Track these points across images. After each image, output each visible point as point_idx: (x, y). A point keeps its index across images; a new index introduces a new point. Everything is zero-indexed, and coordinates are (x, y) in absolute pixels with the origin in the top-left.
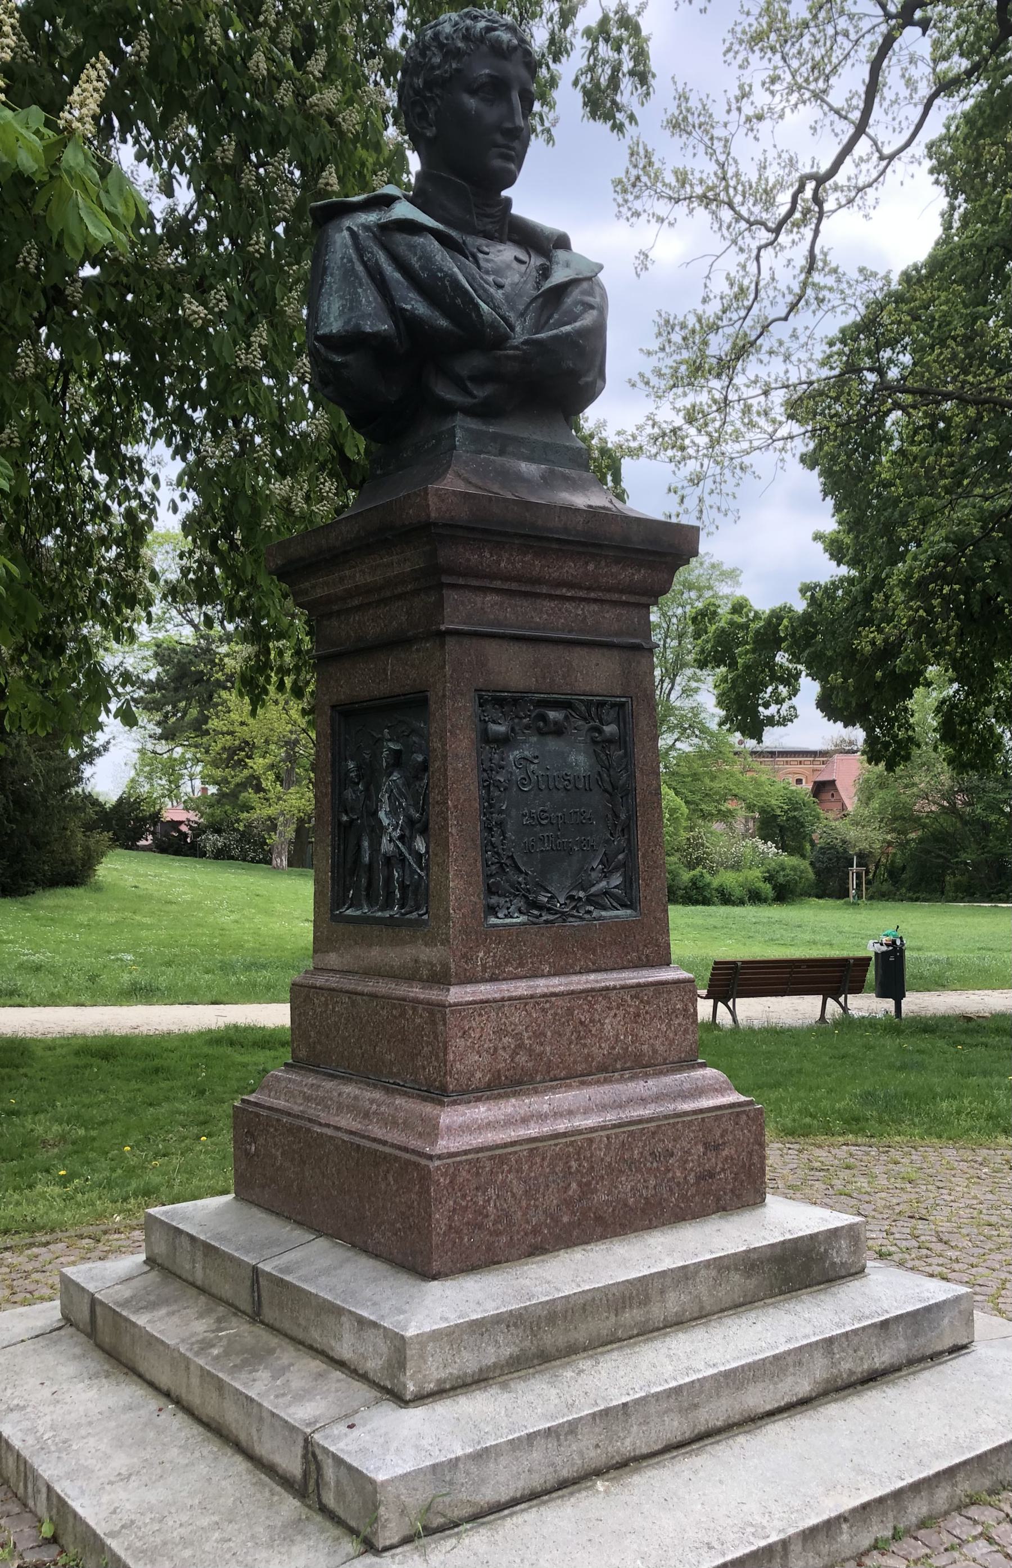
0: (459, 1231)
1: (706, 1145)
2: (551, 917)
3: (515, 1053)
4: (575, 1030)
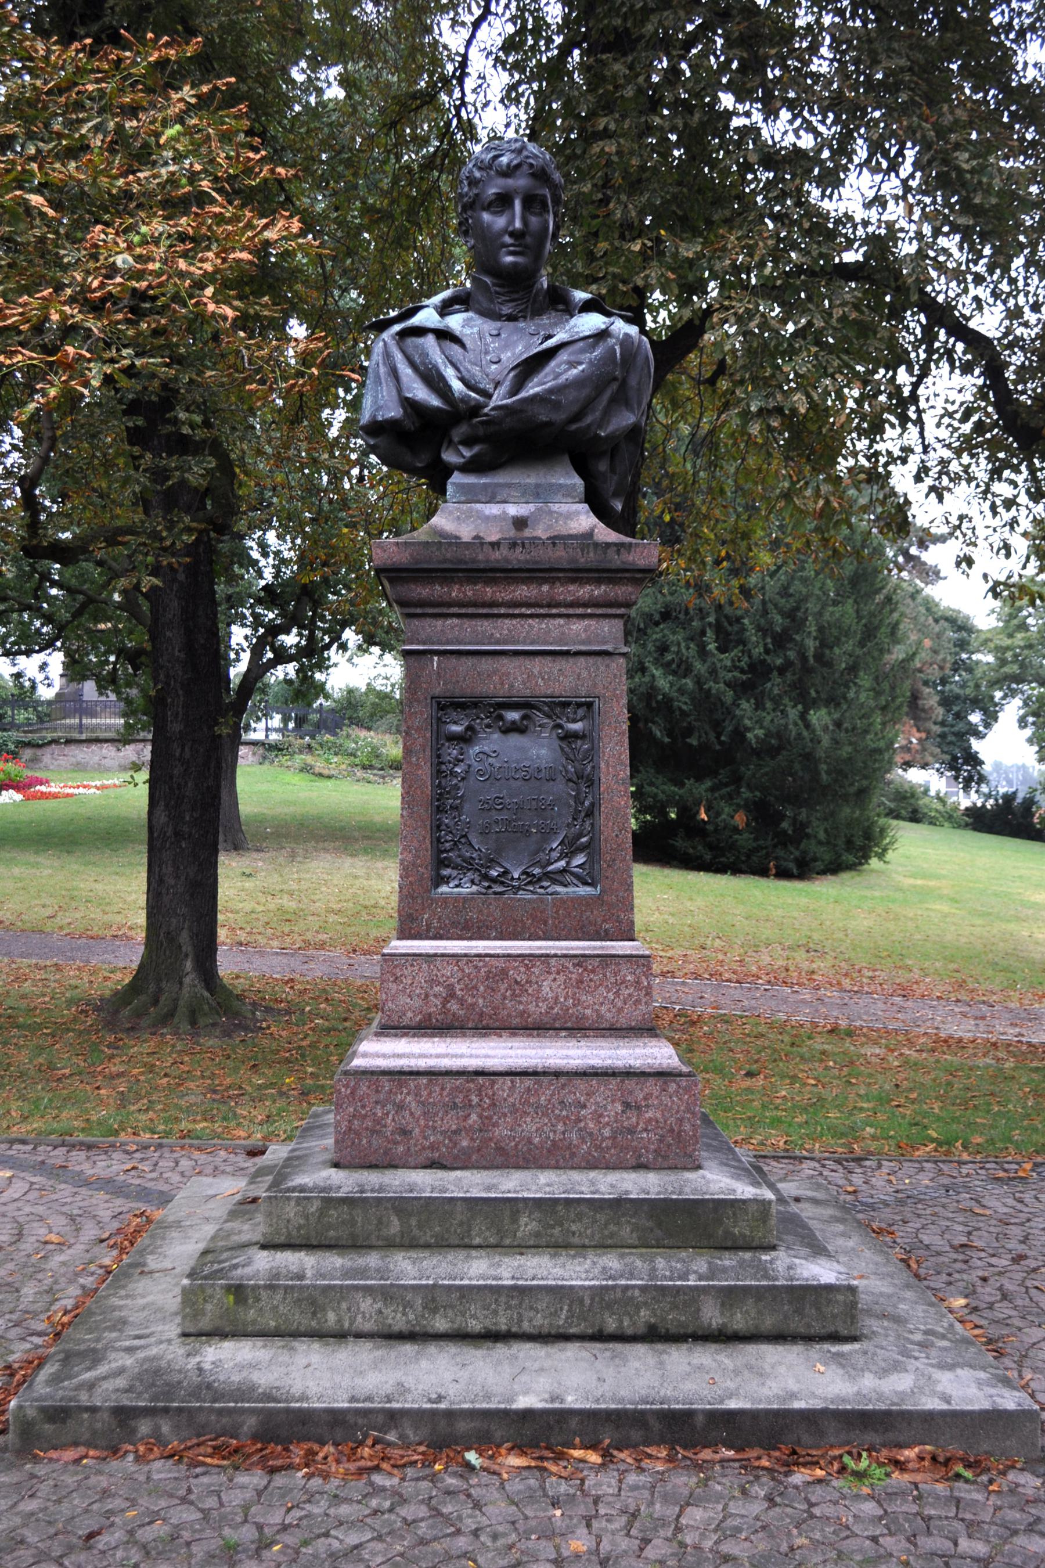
0: (358, 1134)
1: (627, 1105)
2: (501, 889)
3: (445, 1002)
4: (510, 987)
